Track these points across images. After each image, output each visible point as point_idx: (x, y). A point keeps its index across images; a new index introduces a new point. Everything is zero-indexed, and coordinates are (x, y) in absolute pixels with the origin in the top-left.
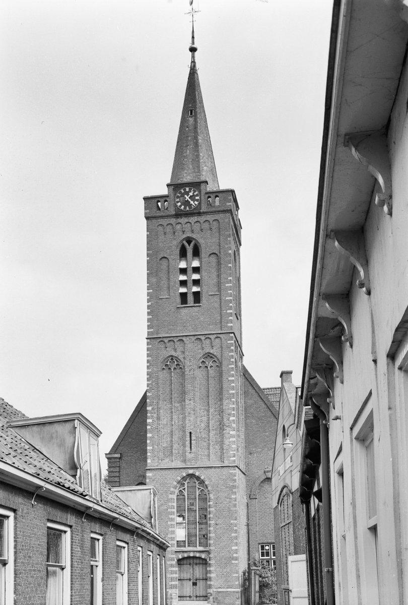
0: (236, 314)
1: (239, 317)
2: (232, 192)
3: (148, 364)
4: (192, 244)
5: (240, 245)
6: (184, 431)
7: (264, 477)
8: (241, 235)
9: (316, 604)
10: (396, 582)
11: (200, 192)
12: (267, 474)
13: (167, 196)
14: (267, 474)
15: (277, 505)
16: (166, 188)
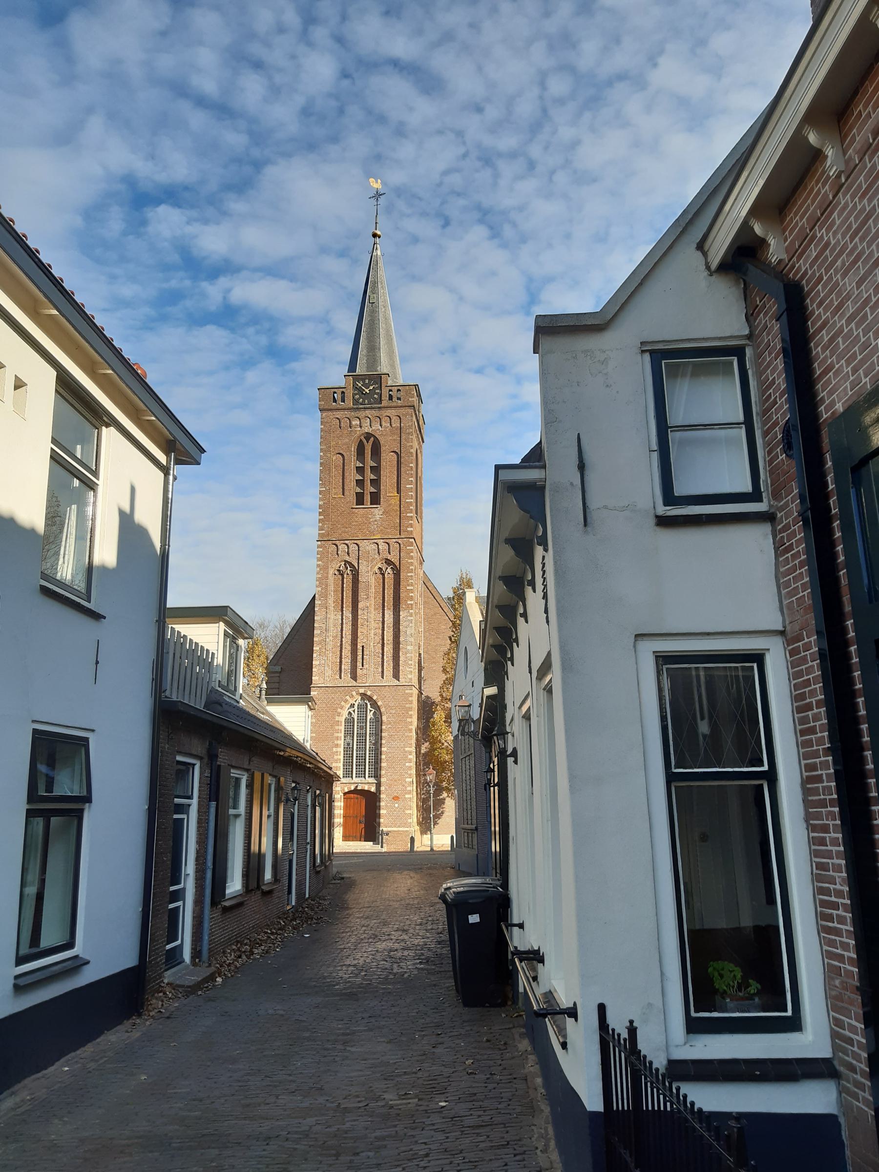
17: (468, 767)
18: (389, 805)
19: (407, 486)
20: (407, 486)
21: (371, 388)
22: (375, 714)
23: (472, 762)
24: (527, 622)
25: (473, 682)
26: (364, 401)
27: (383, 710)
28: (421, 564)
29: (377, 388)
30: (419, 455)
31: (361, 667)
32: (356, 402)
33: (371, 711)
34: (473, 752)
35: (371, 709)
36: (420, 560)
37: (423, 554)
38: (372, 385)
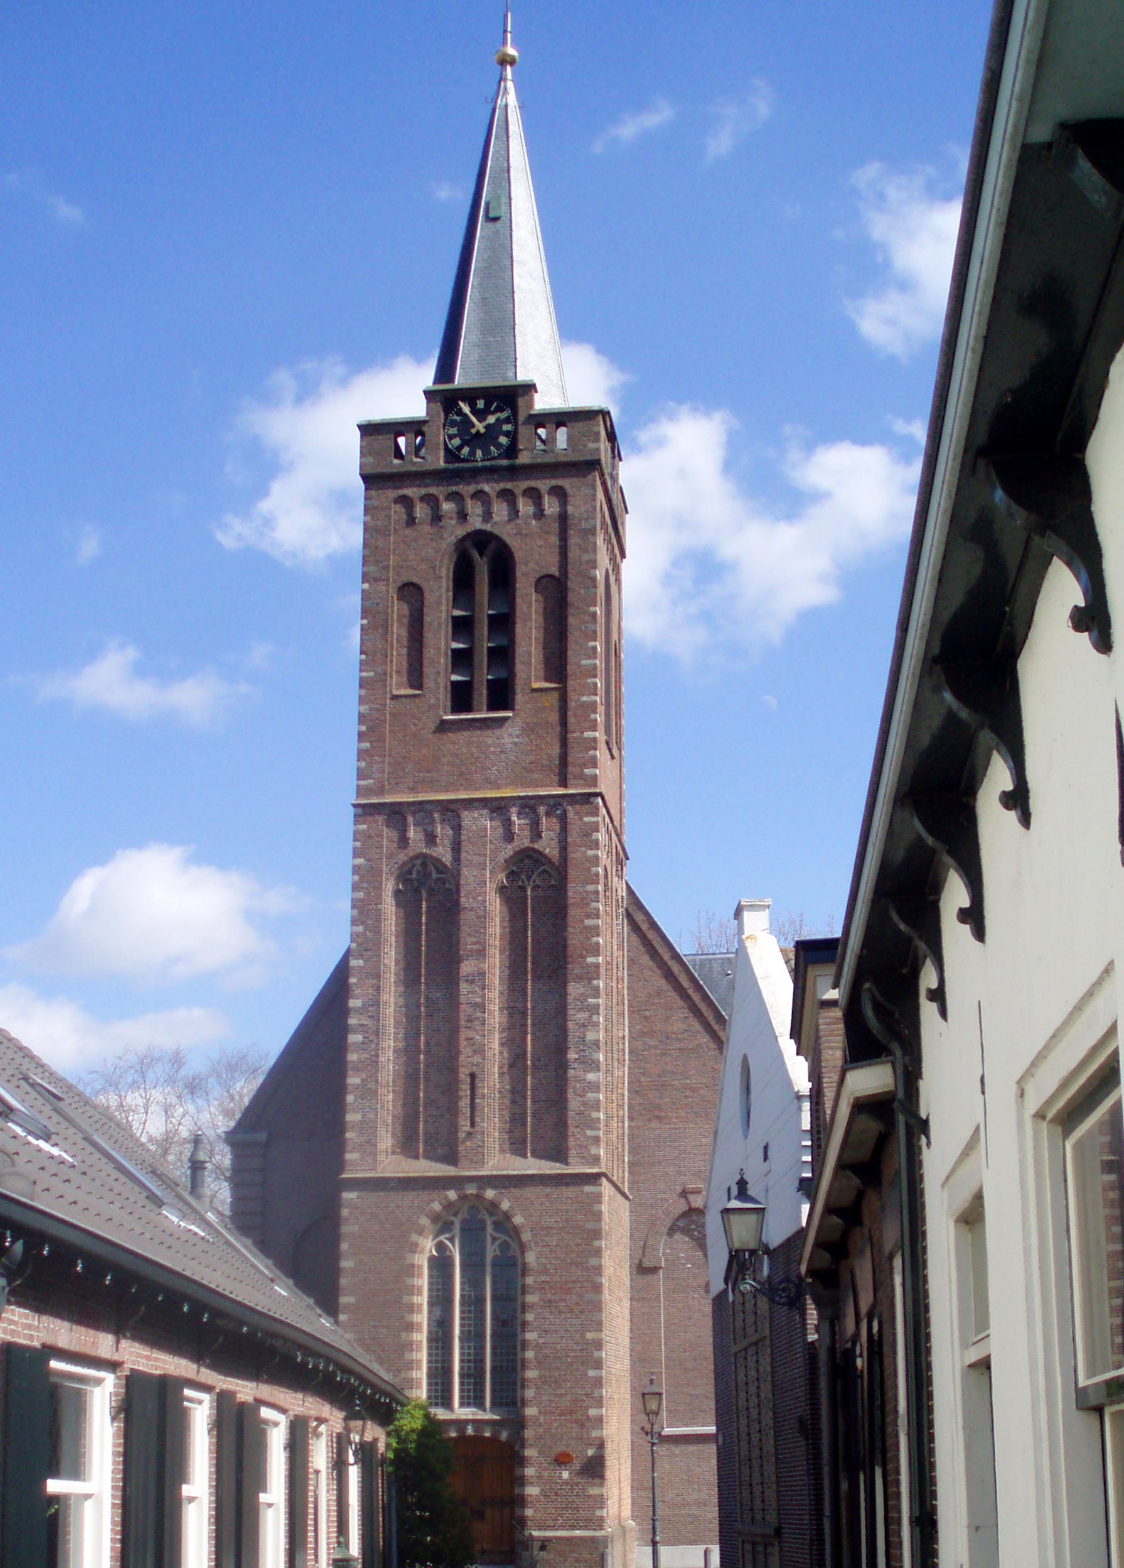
0: (607, 743)
1: (615, 752)
2: (605, 414)
3: (357, 878)
4: (489, 552)
5: (623, 556)
6: (454, 1070)
7: (682, 1207)
8: (624, 532)
9: (846, 1562)
10: (1120, 712)
11: (515, 413)
12: (691, 1198)
13: (423, 422)
14: (691, 1198)
15: (723, 1286)
16: (423, 401)
17: (753, 1373)
18: (546, 1474)
19: (584, 662)
20: (584, 662)
21: (491, 419)
22: (505, 1246)
23: (765, 1361)
24: (943, 1013)
25: (766, 1148)
26: (472, 453)
27: (526, 1237)
28: (620, 863)
29: (507, 421)
30: (614, 588)
31: (468, 1129)
32: (452, 455)
33: (494, 1239)
34: (767, 1332)
35: (497, 1235)
36: (617, 854)
37: (624, 838)
38: (493, 413)
